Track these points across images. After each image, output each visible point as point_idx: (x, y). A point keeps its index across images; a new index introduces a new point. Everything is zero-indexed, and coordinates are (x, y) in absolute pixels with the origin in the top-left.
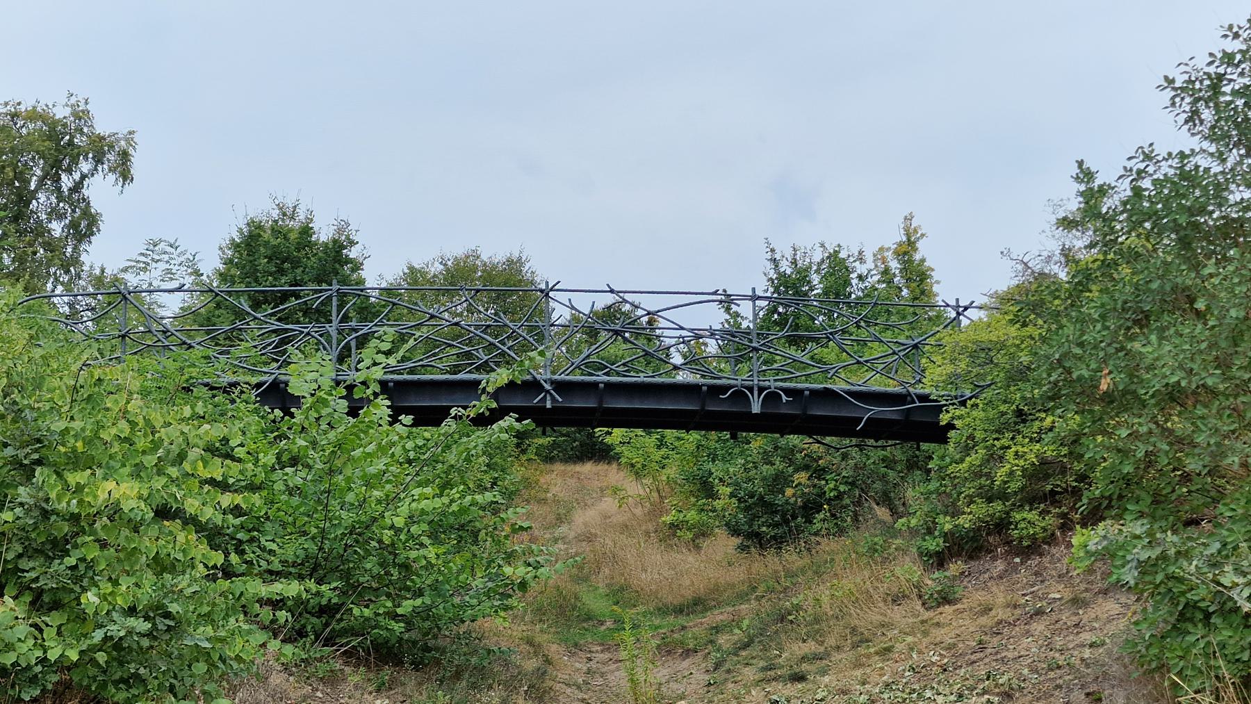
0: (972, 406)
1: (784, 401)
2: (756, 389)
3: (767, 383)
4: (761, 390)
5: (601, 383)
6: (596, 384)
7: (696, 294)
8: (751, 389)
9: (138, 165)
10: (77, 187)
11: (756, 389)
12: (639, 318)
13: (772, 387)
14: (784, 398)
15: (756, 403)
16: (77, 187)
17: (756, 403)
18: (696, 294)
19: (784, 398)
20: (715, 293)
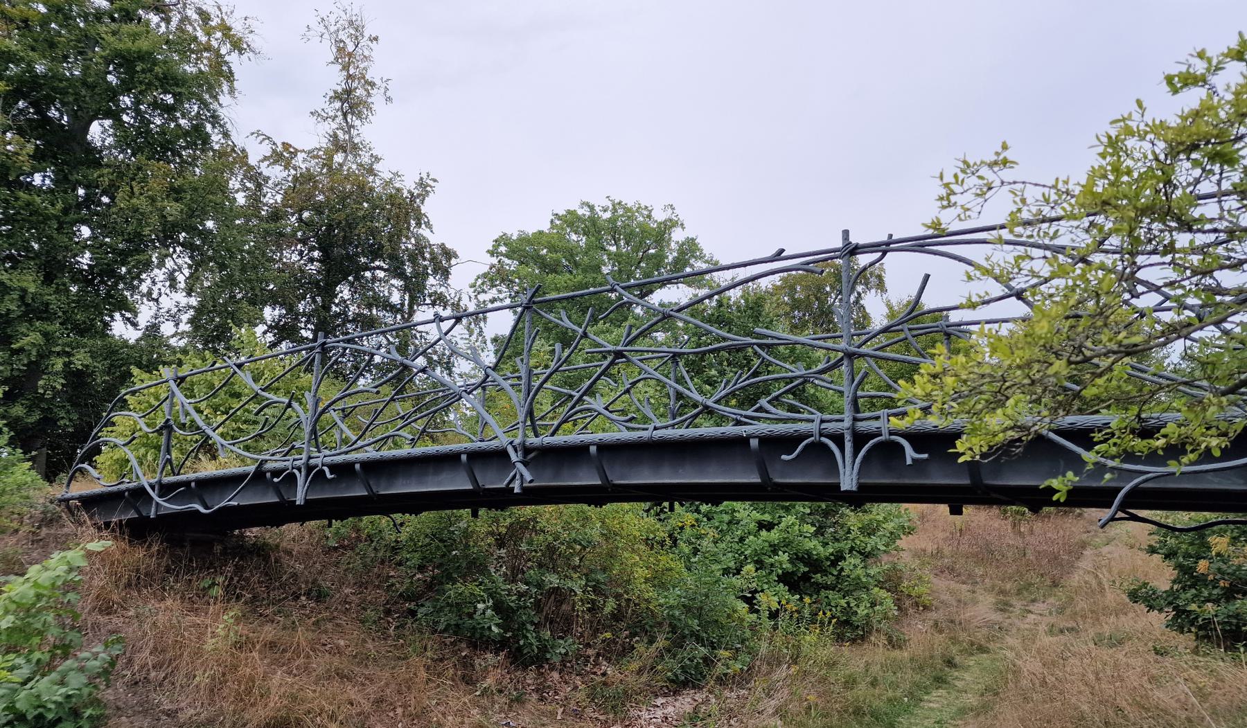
0: (663, 586)
1: (909, 462)
2: (848, 437)
3: (873, 425)
4: (860, 439)
5: (464, 453)
6: (743, 441)
7: (745, 265)
8: (838, 439)
9: (887, 279)
10: (857, 302)
11: (848, 437)
12: (415, 326)
13: (885, 432)
14: (910, 453)
15: (848, 473)
16: (857, 302)
17: (848, 473)
18: (745, 265)
19: (910, 453)
20: (779, 256)
